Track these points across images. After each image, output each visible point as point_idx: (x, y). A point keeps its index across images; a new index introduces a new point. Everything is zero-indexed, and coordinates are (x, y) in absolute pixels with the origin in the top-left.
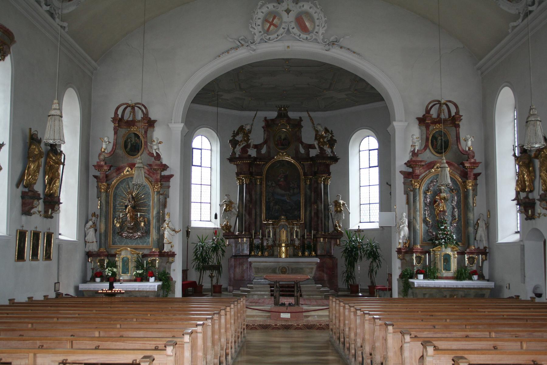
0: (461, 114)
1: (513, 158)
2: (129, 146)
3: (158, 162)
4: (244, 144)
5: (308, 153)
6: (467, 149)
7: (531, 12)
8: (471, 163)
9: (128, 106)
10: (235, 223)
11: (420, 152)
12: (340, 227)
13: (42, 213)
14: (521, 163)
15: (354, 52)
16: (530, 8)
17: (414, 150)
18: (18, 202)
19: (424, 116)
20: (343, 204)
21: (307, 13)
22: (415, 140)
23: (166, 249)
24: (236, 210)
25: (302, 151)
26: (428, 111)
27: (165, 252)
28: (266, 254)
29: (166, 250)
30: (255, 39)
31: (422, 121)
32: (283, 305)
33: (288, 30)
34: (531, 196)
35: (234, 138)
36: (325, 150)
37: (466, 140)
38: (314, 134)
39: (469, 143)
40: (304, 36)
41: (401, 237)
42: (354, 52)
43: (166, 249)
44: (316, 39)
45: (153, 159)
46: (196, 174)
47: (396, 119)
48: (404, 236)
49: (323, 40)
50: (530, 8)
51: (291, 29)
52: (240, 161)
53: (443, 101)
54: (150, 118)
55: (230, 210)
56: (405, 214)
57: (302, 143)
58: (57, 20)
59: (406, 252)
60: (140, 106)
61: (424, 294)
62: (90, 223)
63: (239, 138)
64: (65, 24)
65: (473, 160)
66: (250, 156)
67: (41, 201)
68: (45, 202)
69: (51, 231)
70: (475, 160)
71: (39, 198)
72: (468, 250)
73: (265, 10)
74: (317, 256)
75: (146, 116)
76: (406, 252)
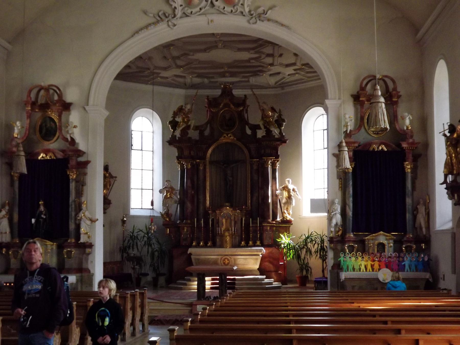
0: (399, 89)
1: (443, 137)
2: (44, 131)
3: (72, 148)
4: (183, 126)
5: (254, 134)
6: (405, 128)
8: (408, 144)
10: (175, 209)
11: (353, 133)
12: (289, 214)
14: (449, 143)
15: (282, 25)
17: (347, 131)
19: (358, 92)
20: (293, 190)
22: (348, 120)
23: (83, 239)
24: (177, 197)
25: (249, 132)
26: (363, 89)
27: (81, 243)
28: (258, 243)
29: (82, 240)
30: (176, 13)
35: (174, 119)
36: (272, 131)
37: (403, 118)
38: (260, 114)
39: (407, 122)
40: (228, 9)
42: (282, 25)
43: (83, 239)
44: (242, 13)
47: (329, 97)
48: (337, 224)
49: (250, 11)
52: (181, 144)
54: (64, 101)
55: (170, 197)
56: (337, 201)
57: (247, 123)
59: (338, 242)
60: (55, 89)
61: (353, 287)
63: (179, 119)
65: (411, 141)
66: (190, 138)
70: (414, 140)
72: (405, 239)
74: (262, 245)
75: (60, 96)
76: (338, 242)
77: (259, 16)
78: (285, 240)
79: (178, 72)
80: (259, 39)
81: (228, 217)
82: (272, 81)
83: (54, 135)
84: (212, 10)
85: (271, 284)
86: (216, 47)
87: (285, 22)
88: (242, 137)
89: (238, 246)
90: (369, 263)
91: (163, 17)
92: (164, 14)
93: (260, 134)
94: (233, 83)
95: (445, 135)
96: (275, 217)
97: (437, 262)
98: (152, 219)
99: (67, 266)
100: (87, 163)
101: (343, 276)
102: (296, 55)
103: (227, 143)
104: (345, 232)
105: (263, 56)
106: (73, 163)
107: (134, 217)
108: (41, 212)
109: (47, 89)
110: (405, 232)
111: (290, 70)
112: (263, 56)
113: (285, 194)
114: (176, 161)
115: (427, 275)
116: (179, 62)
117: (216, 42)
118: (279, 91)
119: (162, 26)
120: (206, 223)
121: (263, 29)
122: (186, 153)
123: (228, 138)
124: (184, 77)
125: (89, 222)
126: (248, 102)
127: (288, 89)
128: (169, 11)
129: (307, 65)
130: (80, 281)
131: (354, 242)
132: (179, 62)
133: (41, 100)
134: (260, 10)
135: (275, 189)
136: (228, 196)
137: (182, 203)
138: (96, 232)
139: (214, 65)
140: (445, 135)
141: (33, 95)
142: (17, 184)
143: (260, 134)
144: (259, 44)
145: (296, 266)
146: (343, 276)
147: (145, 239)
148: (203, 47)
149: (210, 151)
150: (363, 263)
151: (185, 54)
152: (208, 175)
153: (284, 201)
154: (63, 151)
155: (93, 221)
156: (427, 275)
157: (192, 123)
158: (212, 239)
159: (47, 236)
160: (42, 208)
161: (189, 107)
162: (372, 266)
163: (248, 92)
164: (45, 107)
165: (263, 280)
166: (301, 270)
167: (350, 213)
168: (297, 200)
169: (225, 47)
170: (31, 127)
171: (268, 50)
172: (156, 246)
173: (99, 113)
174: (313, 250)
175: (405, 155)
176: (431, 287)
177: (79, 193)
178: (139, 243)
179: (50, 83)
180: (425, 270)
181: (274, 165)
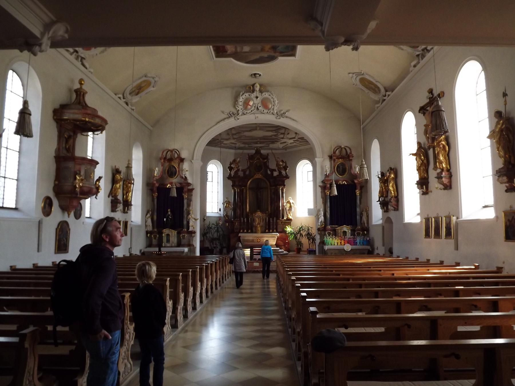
0: (353, 153)
5: (272, 174)
7: (385, 100)
9: (169, 150)
10: (231, 213)
13: (122, 210)
15: (293, 120)
16: (384, 98)
18: (109, 205)
21: (267, 98)
22: (327, 169)
23: (191, 229)
25: (269, 172)
26: (334, 153)
28: (275, 231)
29: (190, 230)
31: (331, 157)
32: (255, 259)
33: (257, 108)
34: (386, 199)
37: (355, 168)
38: (275, 163)
39: (357, 170)
40: (266, 111)
41: (320, 221)
42: (293, 120)
43: (191, 229)
45: (183, 180)
46: (209, 185)
50: (384, 98)
51: (259, 108)
52: (234, 179)
53: (342, 146)
56: (321, 210)
57: (269, 168)
58: (129, 105)
59: (322, 230)
61: (332, 253)
62: (149, 215)
64: (133, 108)
67: (121, 205)
68: (123, 205)
69: (127, 220)
71: (120, 203)
73: (244, 96)
75: (179, 156)
76: (322, 230)
77: (282, 115)
78: (289, 229)
79: (233, 141)
80: (279, 126)
81: (259, 217)
82: (281, 146)
83: (175, 175)
84: (258, 112)
85: (283, 252)
86: (256, 129)
87: (294, 118)
88: (266, 175)
89: (265, 232)
90: (339, 241)
91: (232, 115)
92: (233, 113)
93: (276, 174)
94: (261, 147)
95: (379, 177)
96: (283, 217)
97: (373, 240)
98: (220, 218)
99: (182, 243)
100: (192, 189)
101: (326, 248)
102: (296, 133)
103: (257, 179)
104: (326, 225)
105: (279, 134)
106: (185, 189)
107: (209, 217)
108: (169, 215)
109: (171, 151)
110: (356, 225)
111: (292, 141)
112: (279, 134)
113: (288, 205)
114: (231, 188)
115: (369, 247)
116: (235, 137)
117: (256, 127)
118: (284, 151)
119: (232, 119)
120: (248, 220)
121: (282, 121)
122: (237, 183)
123: (258, 176)
124: (236, 144)
125: (194, 220)
126: (269, 157)
127: (288, 150)
128: (235, 112)
129: (302, 138)
130: (190, 251)
131: (330, 230)
132: (235, 137)
133: (169, 156)
134: (282, 112)
135: (283, 203)
136: (258, 206)
137: (234, 210)
138: (196, 227)
139: (252, 138)
140: (379, 177)
141: (164, 154)
142: (156, 200)
143: (276, 174)
144: (277, 128)
145: (295, 242)
146: (326, 248)
147: (216, 229)
148: (249, 129)
149: (249, 182)
150: (336, 241)
151: (239, 133)
152: (248, 195)
153: (288, 209)
154: (180, 184)
155: (196, 220)
156: (369, 247)
157: (241, 168)
158: (251, 229)
159: (173, 228)
160: (169, 213)
161: (238, 159)
162: (341, 243)
163: (270, 151)
164: (171, 160)
165: (278, 250)
166: (298, 245)
167: (328, 215)
168: (294, 208)
169: (260, 129)
170: (163, 171)
171: (282, 131)
172: (221, 233)
173: (198, 163)
174: (304, 235)
175: (356, 186)
176: (370, 253)
177: (189, 205)
178: (212, 231)
179: (173, 148)
180: (367, 245)
181: (282, 190)
